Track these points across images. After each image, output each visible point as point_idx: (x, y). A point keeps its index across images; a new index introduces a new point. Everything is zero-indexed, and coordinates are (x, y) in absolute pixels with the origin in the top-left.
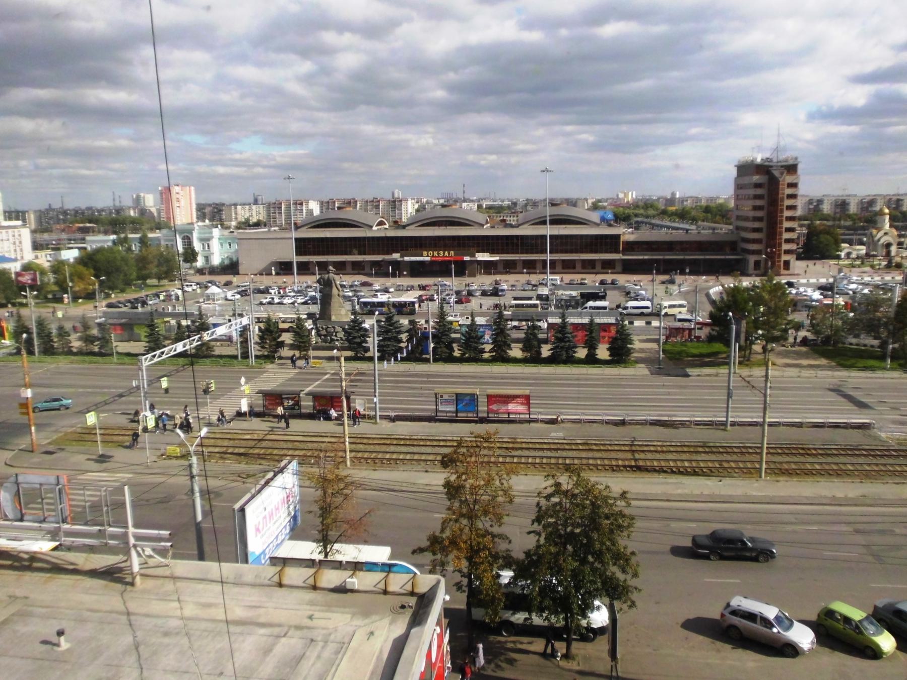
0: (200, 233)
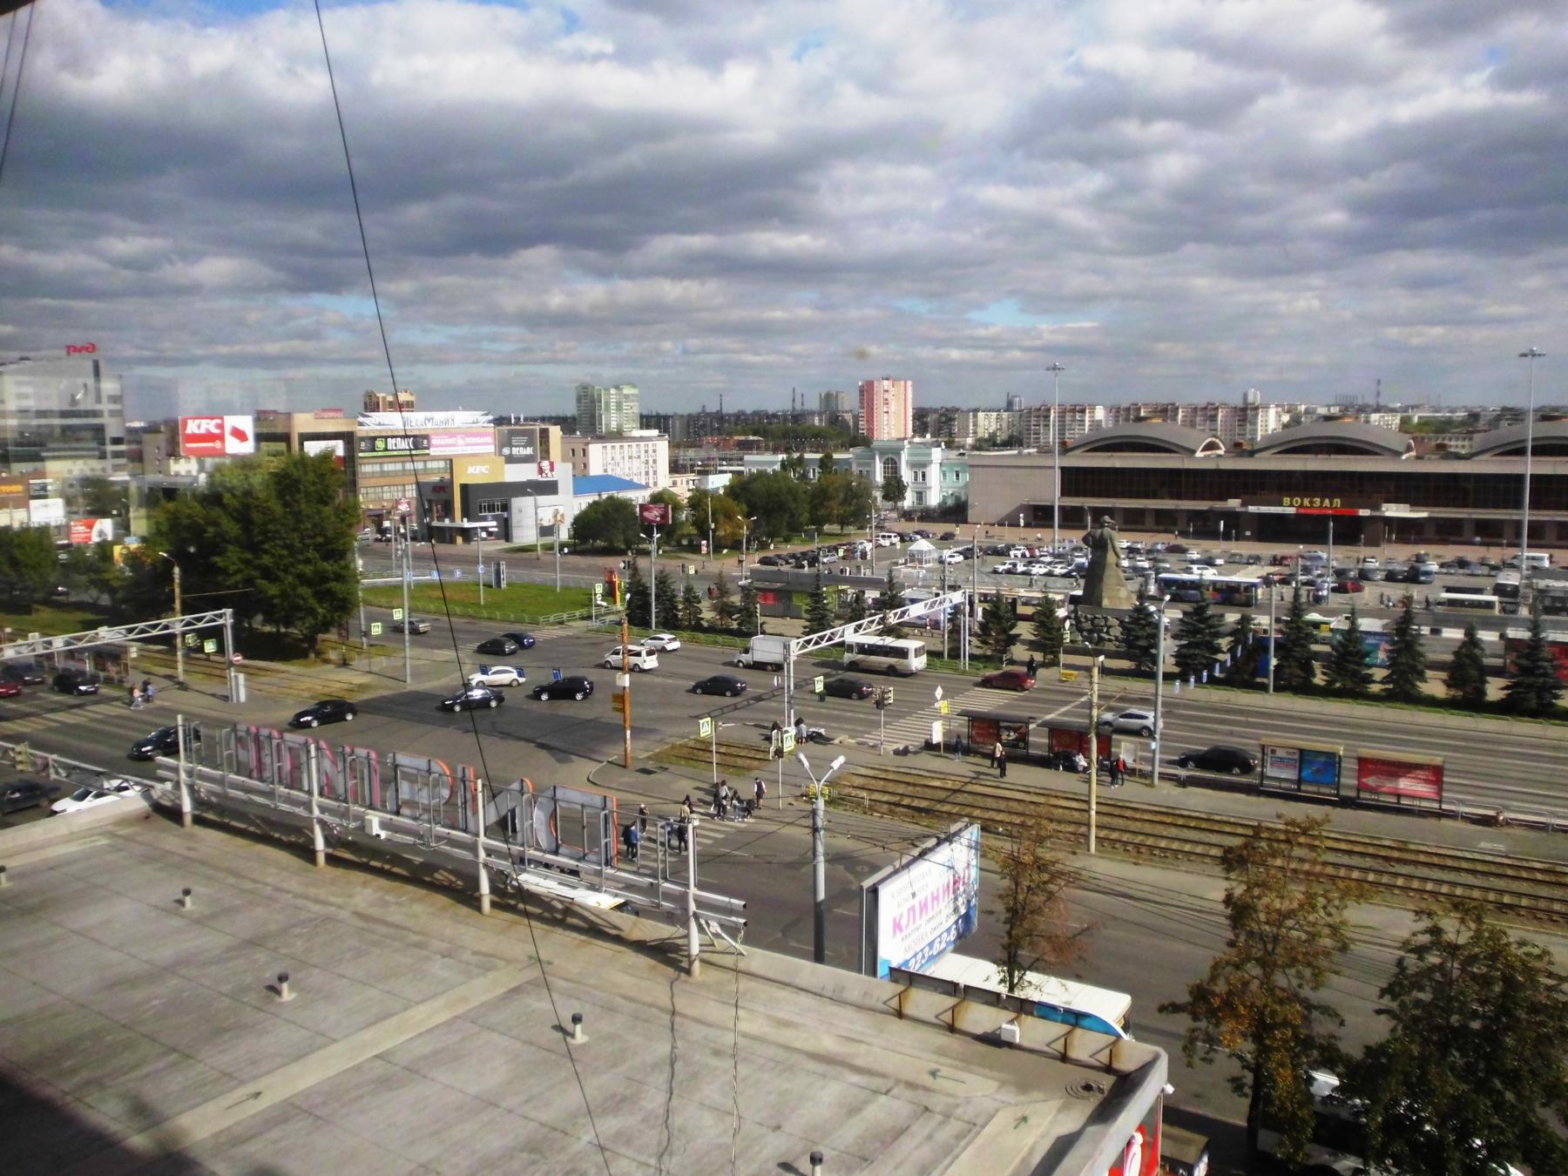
0: (910, 455)
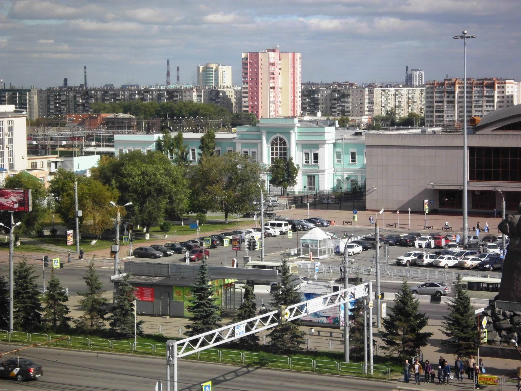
0: (301, 134)
